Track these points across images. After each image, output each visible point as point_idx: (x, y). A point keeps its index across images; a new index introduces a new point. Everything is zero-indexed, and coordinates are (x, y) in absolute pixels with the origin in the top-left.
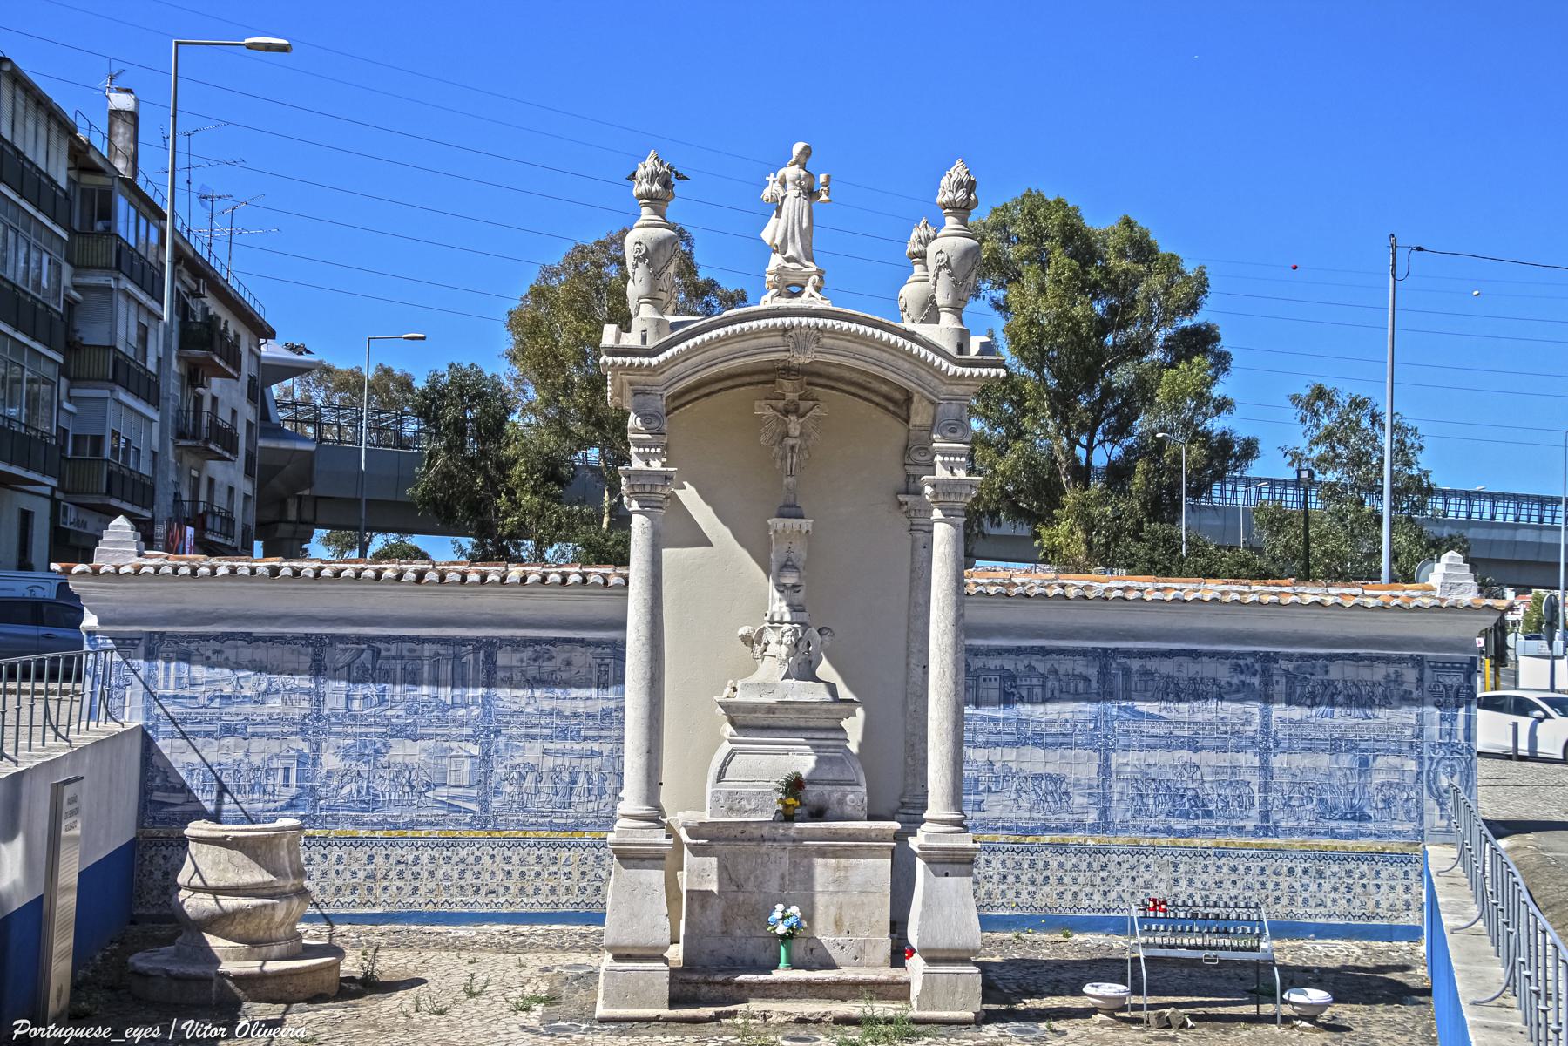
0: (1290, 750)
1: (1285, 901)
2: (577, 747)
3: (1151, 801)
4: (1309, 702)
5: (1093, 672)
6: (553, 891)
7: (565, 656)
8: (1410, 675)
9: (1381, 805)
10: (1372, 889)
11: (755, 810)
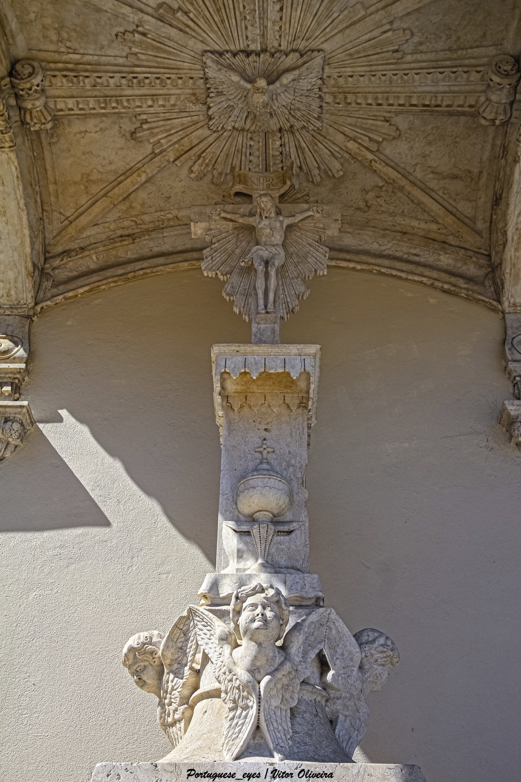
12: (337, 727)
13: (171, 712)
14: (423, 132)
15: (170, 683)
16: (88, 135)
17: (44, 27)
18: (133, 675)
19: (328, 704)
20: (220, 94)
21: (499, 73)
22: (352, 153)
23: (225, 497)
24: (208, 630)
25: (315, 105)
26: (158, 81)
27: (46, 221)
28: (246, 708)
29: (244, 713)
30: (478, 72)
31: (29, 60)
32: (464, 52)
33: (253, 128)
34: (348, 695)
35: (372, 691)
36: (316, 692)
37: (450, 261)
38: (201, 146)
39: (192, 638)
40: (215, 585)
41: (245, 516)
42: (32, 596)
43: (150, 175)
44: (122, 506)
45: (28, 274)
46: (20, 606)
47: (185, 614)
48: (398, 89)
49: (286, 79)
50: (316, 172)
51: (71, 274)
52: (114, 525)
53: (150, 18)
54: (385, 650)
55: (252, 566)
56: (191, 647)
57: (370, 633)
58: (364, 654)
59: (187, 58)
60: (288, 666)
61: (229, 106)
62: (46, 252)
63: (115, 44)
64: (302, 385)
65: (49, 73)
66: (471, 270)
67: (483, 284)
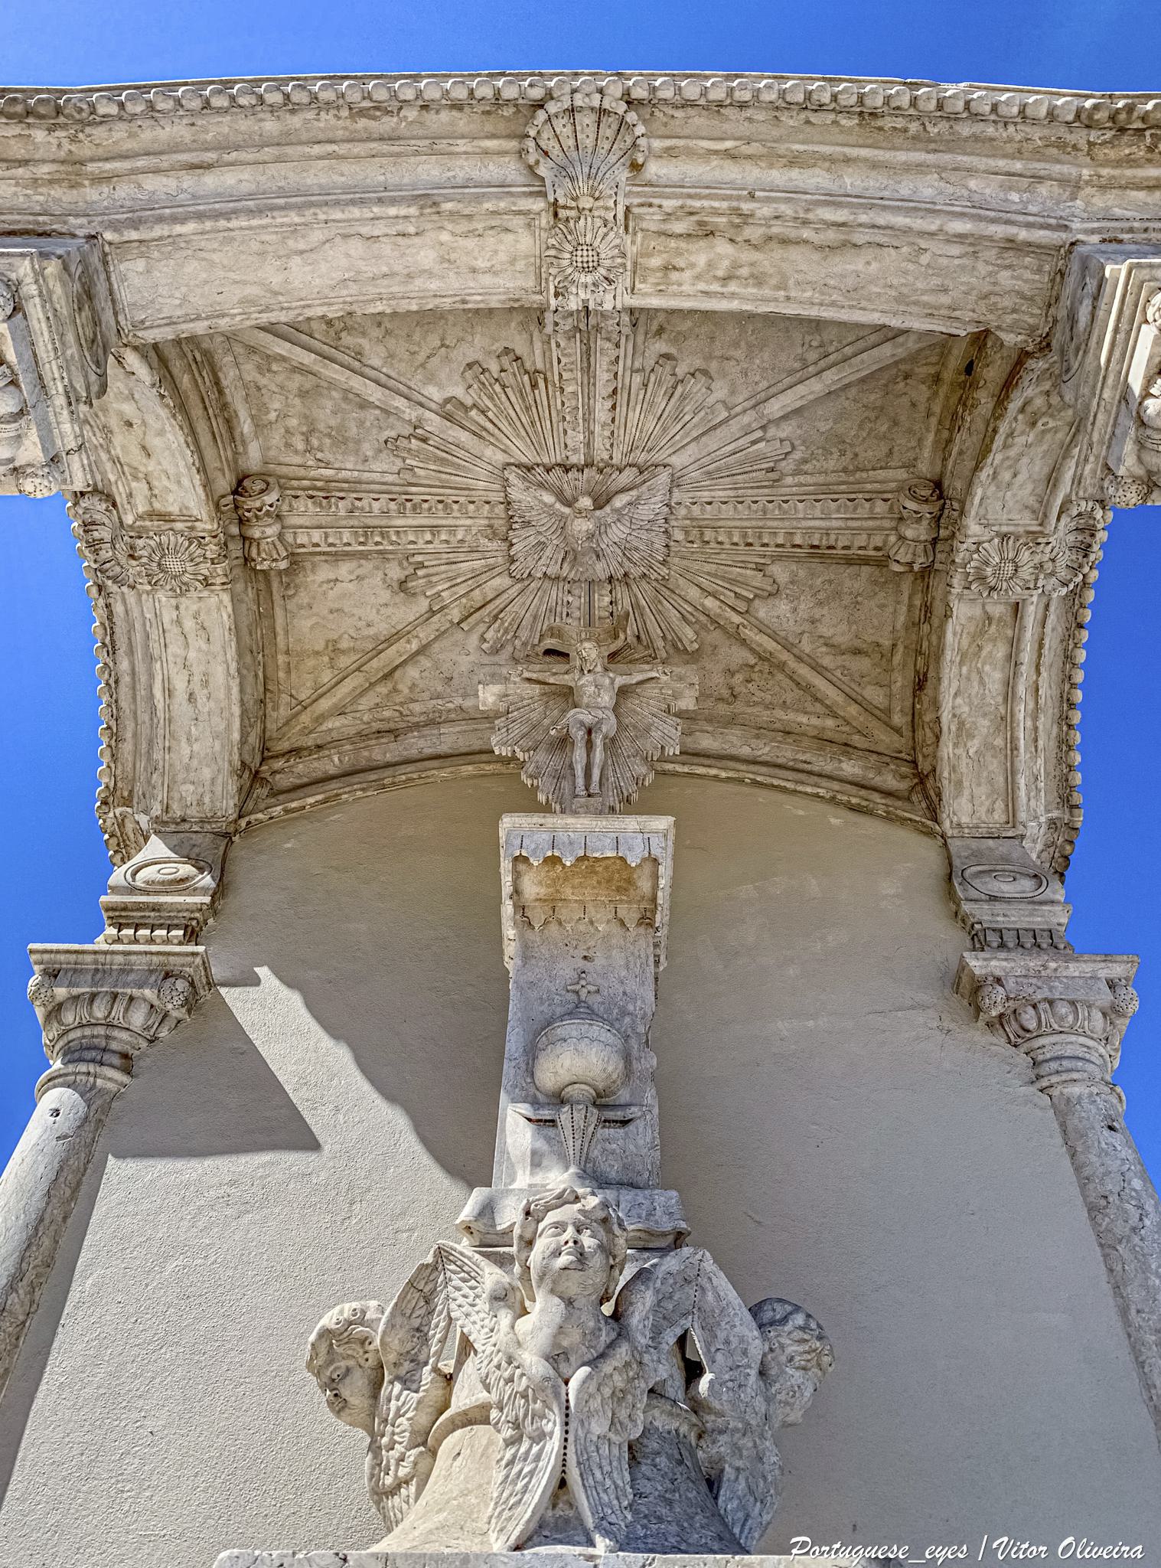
12: (722, 1492)
13: (392, 1462)
14: (811, 587)
15: (393, 1402)
16: (339, 584)
17: (287, 431)
18: (324, 1387)
19: (702, 1443)
20: (527, 524)
21: (914, 498)
22: (712, 614)
23: (513, 1064)
24: (471, 1288)
25: (659, 542)
26: (440, 506)
27: (270, 705)
28: (541, 1437)
29: (535, 1449)
30: (885, 500)
31: (263, 476)
32: (864, 475)
33: (572, 575)
34: (740, 1425)
35: (786, 1425)
36: (678, 1415)
37: (857, 771)
38: (497, 602)
39: (439, 1308)
40: (487, 1210)
41: (547, 1095)
42: (170, 1267)
43: (424, 642)
44: (341, 1117)
45: (233, 772)
46: (147, 1285)
47: (429, 1259)
48: (775, 524)
49: (619, 502)
50: (660, 643)
51: (298, 782)
52: (326, 1148)
53: (433, 416)
54: (806, 1337)
55: (558, 1178)
56: (437, 1326)
57: (777, 1306)
58: (767, 1348)
59: (482, 474)
60: (623, 1352)
61: (539, 543)
62: (265, 748)
63: (383, 455)
64: (645, 885)
65: (289, 492)
66: (890, 781)
67: (908, 799)
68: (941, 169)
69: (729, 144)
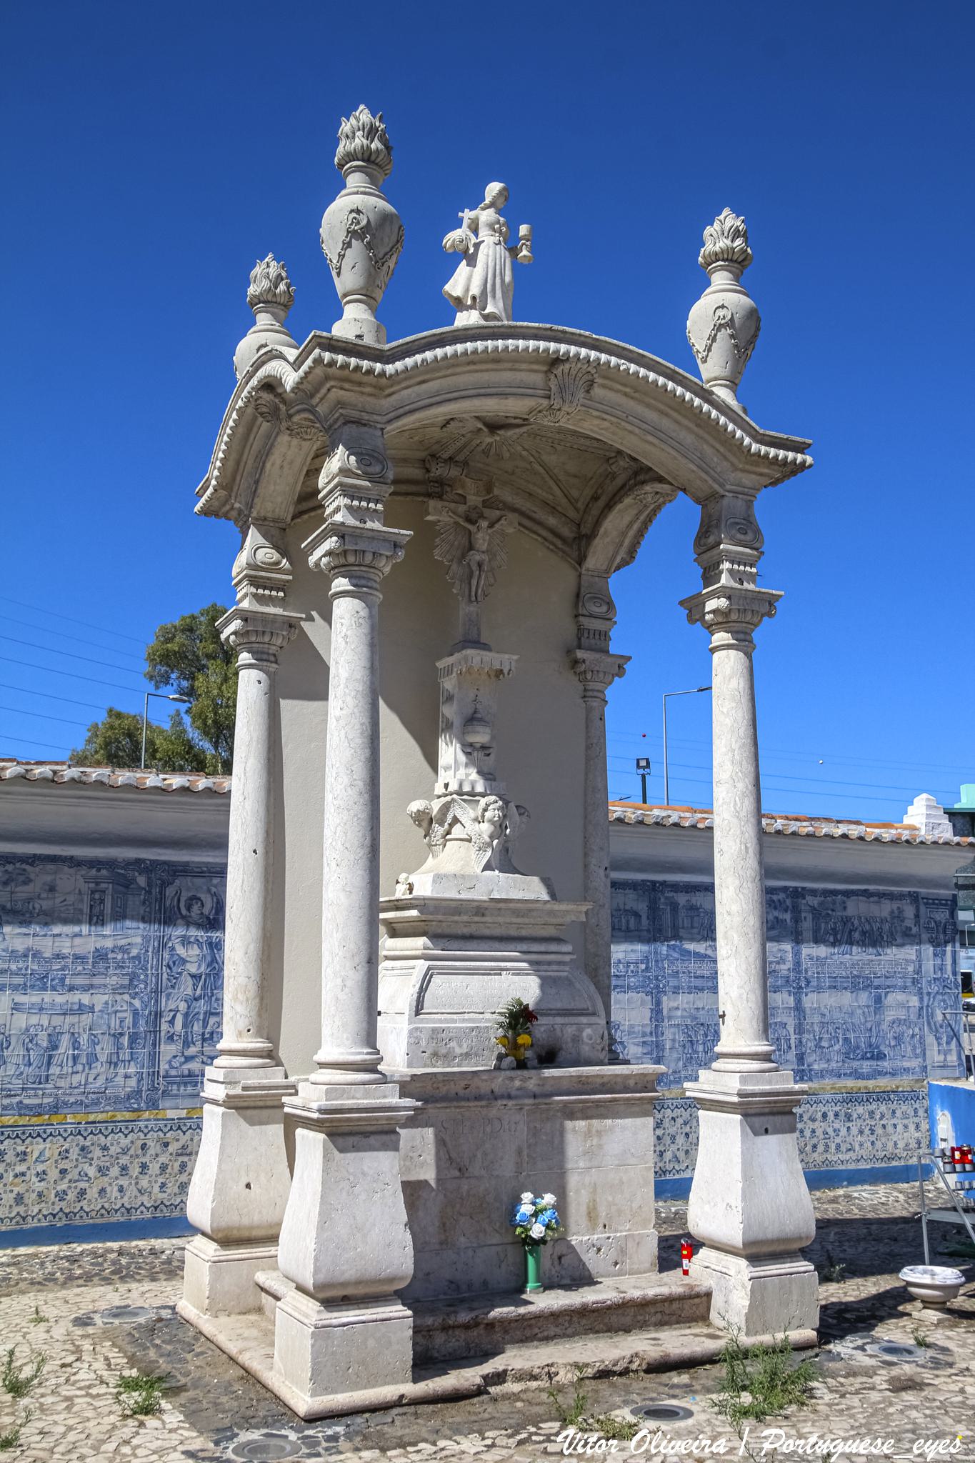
0: (819, 989)
1: (821, 1148)
2: (60, 999)
3: (701, 1048)
4: (831, 939)
5: (642, 907)
6: (19, 1199)
7: (49, 878)
8: (909, 911)
9: (893, 1043)
10: (890, 1129)
11: (467, 1055)
68: (697, 435)
69: (628, 390)
